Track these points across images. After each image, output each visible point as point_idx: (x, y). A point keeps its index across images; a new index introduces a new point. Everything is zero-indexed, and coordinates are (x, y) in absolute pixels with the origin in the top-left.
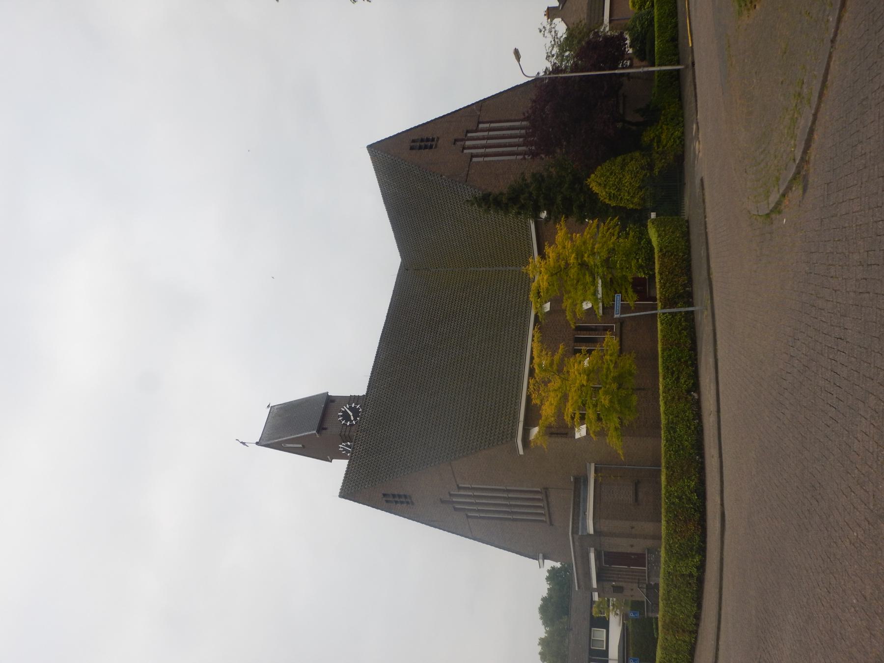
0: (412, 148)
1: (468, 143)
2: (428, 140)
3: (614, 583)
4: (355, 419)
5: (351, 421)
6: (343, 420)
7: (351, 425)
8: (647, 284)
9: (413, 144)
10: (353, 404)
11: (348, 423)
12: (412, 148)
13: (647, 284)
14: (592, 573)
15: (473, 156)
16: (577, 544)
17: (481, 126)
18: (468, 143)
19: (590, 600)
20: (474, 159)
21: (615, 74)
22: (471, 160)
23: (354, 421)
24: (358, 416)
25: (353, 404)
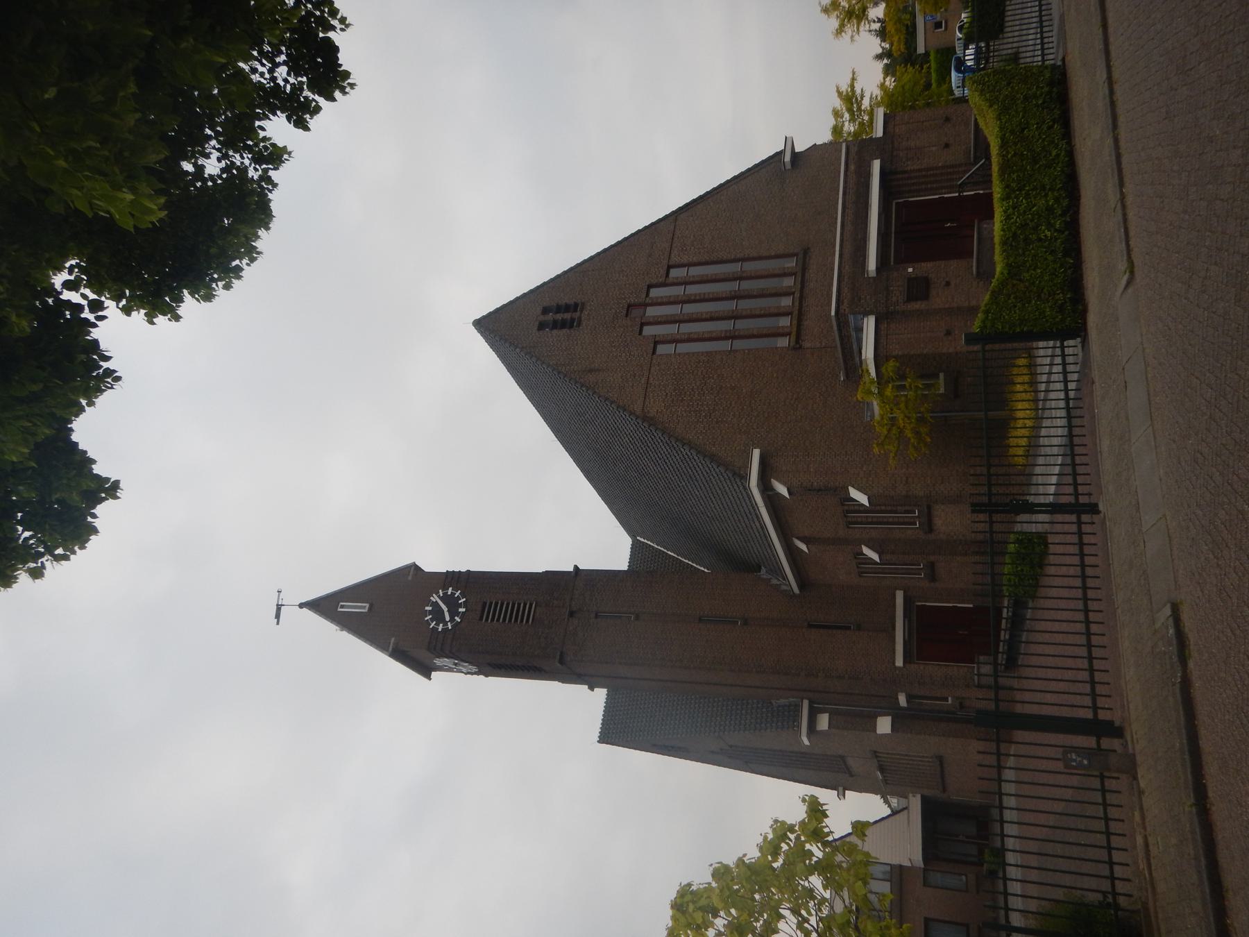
0: (542, 326)
1: (652, 312)
2: (567, 308)
3: (910, 270)
4: (452, 620)
5: (445, 623)
6: (432, 620)
7: (445, 630)
8: (977, 166)
9: (542, 318)
10: (450, 589)
11: (440, 628)
12: (542, 326)
13: (977, 166)
14: (873, 198)
15: (657, 342)
16: (852, 167)
17: (674, 273)
18: (652, 312)
19: (893, 817)
20: (661, 349)
21: (956, 606)
22: (654, 352)
23: (449, 623)
24: (458, 614)
25: (450, 589)
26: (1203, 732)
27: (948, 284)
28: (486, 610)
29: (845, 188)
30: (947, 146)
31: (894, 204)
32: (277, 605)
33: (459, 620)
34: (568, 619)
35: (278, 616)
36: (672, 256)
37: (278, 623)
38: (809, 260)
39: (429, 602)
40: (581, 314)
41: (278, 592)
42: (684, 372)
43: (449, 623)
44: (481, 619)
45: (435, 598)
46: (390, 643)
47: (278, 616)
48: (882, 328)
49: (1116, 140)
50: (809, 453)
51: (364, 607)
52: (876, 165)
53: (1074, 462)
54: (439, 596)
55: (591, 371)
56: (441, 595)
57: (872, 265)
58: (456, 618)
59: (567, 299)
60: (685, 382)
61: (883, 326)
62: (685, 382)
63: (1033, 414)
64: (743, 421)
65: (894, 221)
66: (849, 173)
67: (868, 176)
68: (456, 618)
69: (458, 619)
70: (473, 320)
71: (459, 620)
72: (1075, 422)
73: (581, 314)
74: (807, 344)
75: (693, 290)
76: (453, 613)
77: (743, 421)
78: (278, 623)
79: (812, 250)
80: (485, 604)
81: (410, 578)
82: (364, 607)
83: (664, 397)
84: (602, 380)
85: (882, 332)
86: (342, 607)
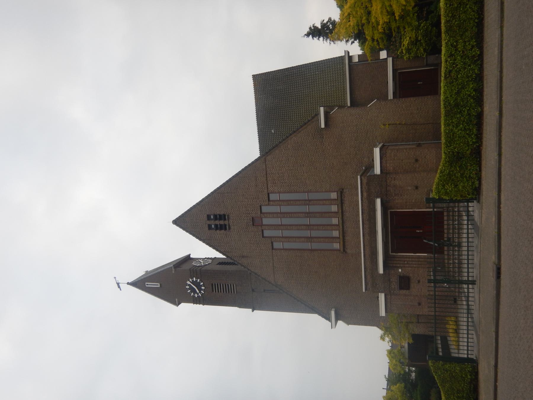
23: (199, 294)
26: (502, 169)
27: (419, 282)
28: (214, 288)
29: (362, 210)
30: (417, 188)
31: (389, 213)
32: (117, 283)
33: (202, 283)
34: (252, 293)
35: (119, 287)
36: (269, 187)
37: (121, 290)
38: (344, 197)
39: (187, 285)
40: (229, 221)
41: (115, 278)
42: (290, 261)
43: (199, 294)
44: (213, 291)
45: (189, 283)
46: (176, 301)
47: (119, 287)
48: (388, 298)
49: (502, 35)
50: (356, 309)
51: (158, 285)
52: (378, 201)
53: (468, 287)
54: (190, 282)
55: (243, 257)
56: (191, 281)
57: (381, 271)
58: (201, 284)
59: (219, 211)
60: (292, 267)
61: (389, 297)
62: (292, 267)
63: (456, 339)
64: (324, 290)
65: (389, 227)
66: (363, 199)
67: (374, 210)
68: (201, 284)
69: (202, 292)
70: (172, 224)
71: (202, 283)
72: (470, 249)
73: (229, 221)
74: (349, 251)
75: (285, 209)
76: (200, 290)
77: (324, 290)
78: (121, 290)
79: (345, 191)
80: (212, 285)
81: (173, 272)
82: (158, 285)
83: (283, 274)
84: (250, 262)
85: (388, 300)
86: (147, 285)
